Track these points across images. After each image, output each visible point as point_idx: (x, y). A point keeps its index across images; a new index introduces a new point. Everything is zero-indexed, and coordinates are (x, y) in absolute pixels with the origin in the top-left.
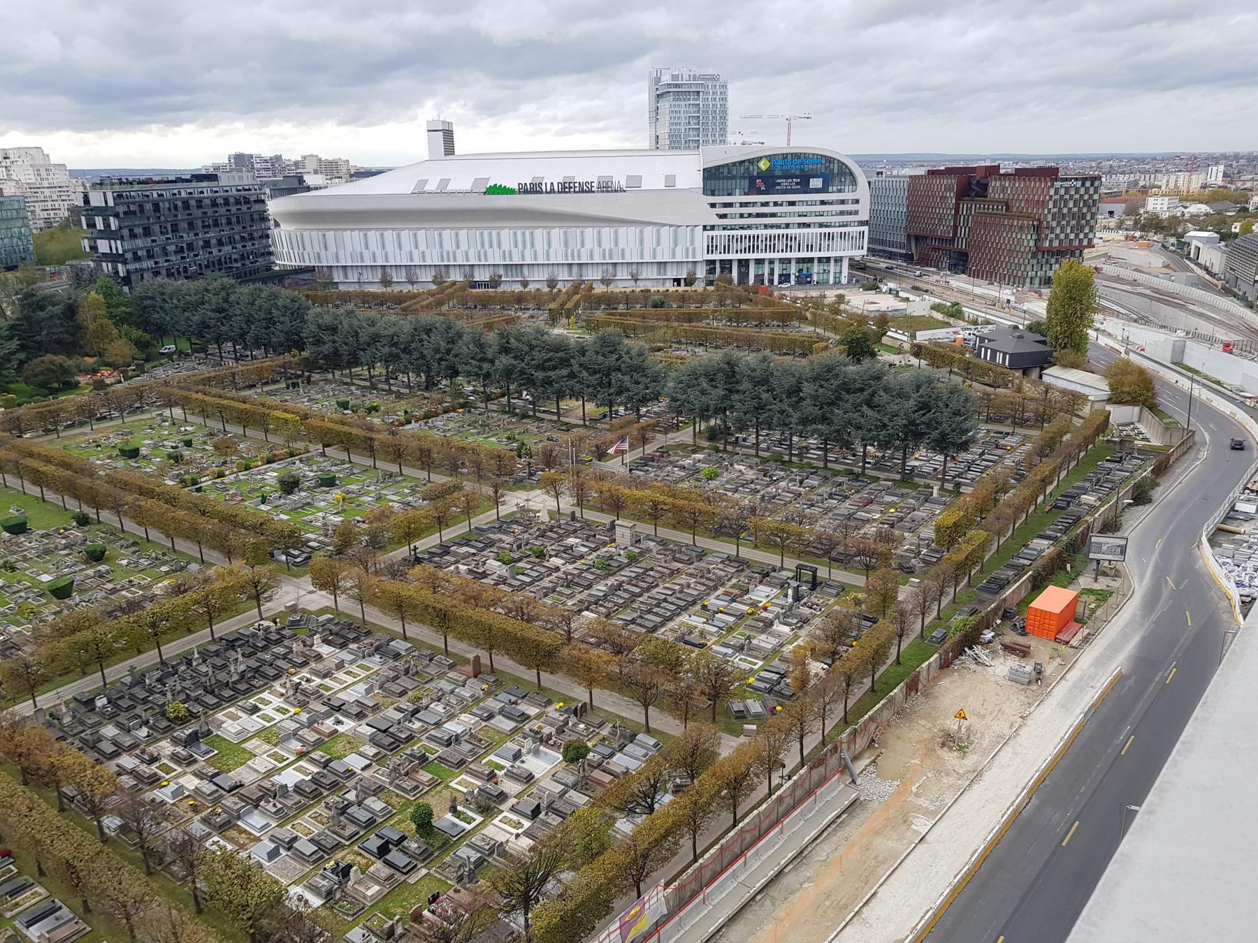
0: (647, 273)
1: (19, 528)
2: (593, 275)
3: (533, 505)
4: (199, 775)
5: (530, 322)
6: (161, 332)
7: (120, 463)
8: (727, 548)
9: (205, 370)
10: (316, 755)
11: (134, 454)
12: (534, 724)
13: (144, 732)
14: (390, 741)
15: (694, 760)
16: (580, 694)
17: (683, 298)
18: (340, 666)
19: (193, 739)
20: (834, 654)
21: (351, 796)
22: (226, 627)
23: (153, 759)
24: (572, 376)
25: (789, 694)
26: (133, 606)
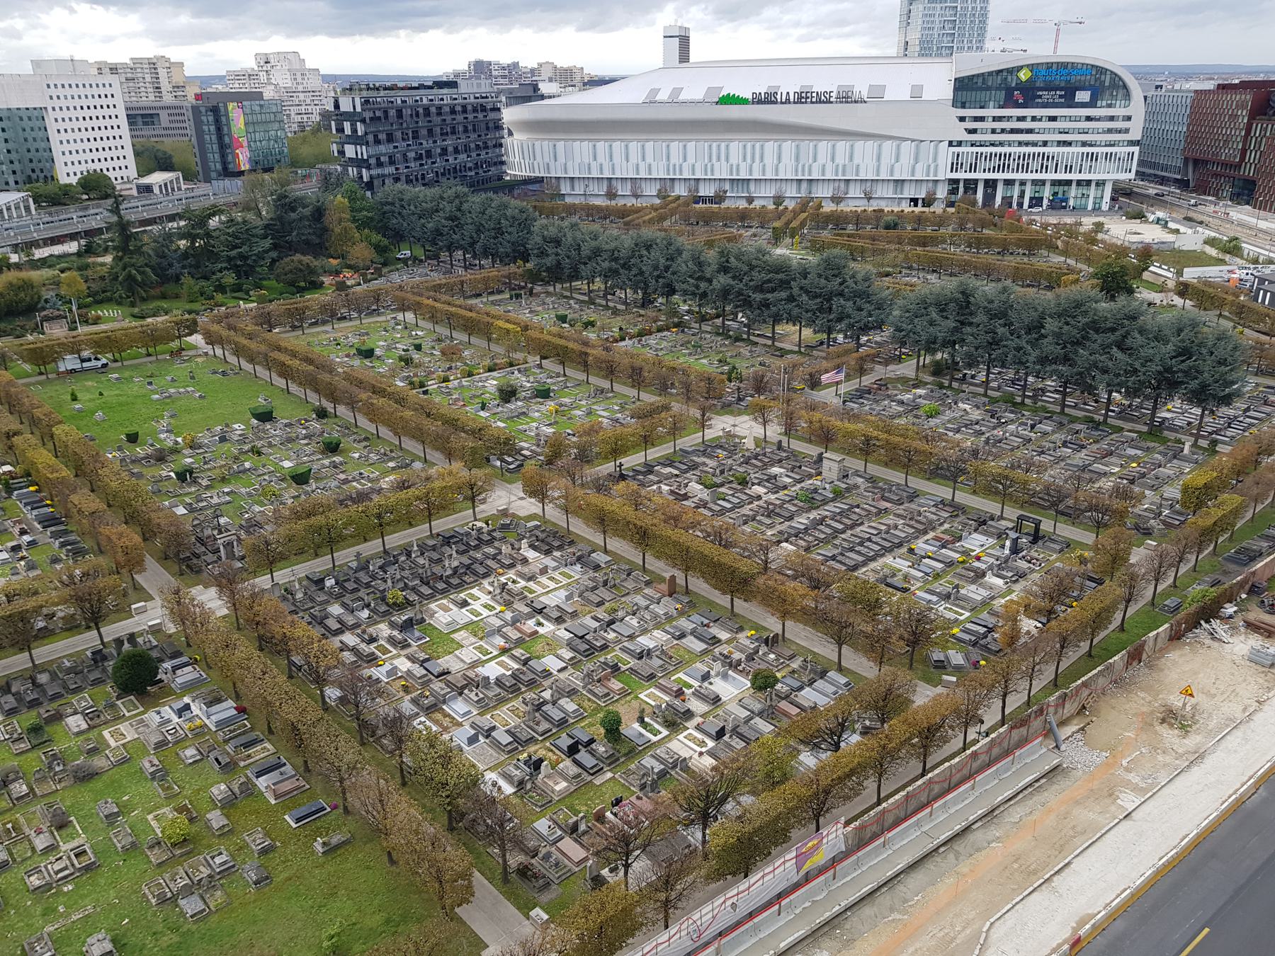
0: (881, 191)
1: (265, 416)
2: (823, 192)
3: (739, 431)
4: (412, 659)
5: (752, 240)
7: (357, 362)
8: (944, 491)
9: (437, 277)
10: (518, 652)
11: (369, 354)
12: (725, 649)
13: (365, 614)
14: (585, 648)
15: (887, 704)
16: (773, 624)
17: (919, 220)
18: (544, 571)
19: (408, 625)
20: (1050, 613)
21: (547, 695)
22: (443, 524)
23: (372, 640)
24: (791, 299)
25: (996, 651)
26: (362, 497)
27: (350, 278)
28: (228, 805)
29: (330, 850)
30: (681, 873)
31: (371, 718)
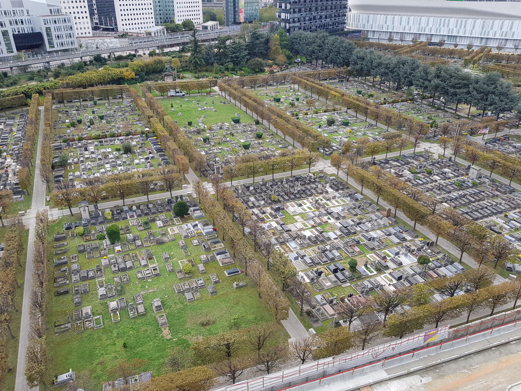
1: (237, 121)
4: (277, 223)
7: (273, 103)
10: (319, 228)
11: (278, 100)
13: (263, 202)
18: (334, 198)
19: (278, 210)
21: (328, 247)
22: (297, 172)
23: (264, 213)
26: (267, 157)
28: (206, 263)
29: (239, 287)
31: (259, 242)
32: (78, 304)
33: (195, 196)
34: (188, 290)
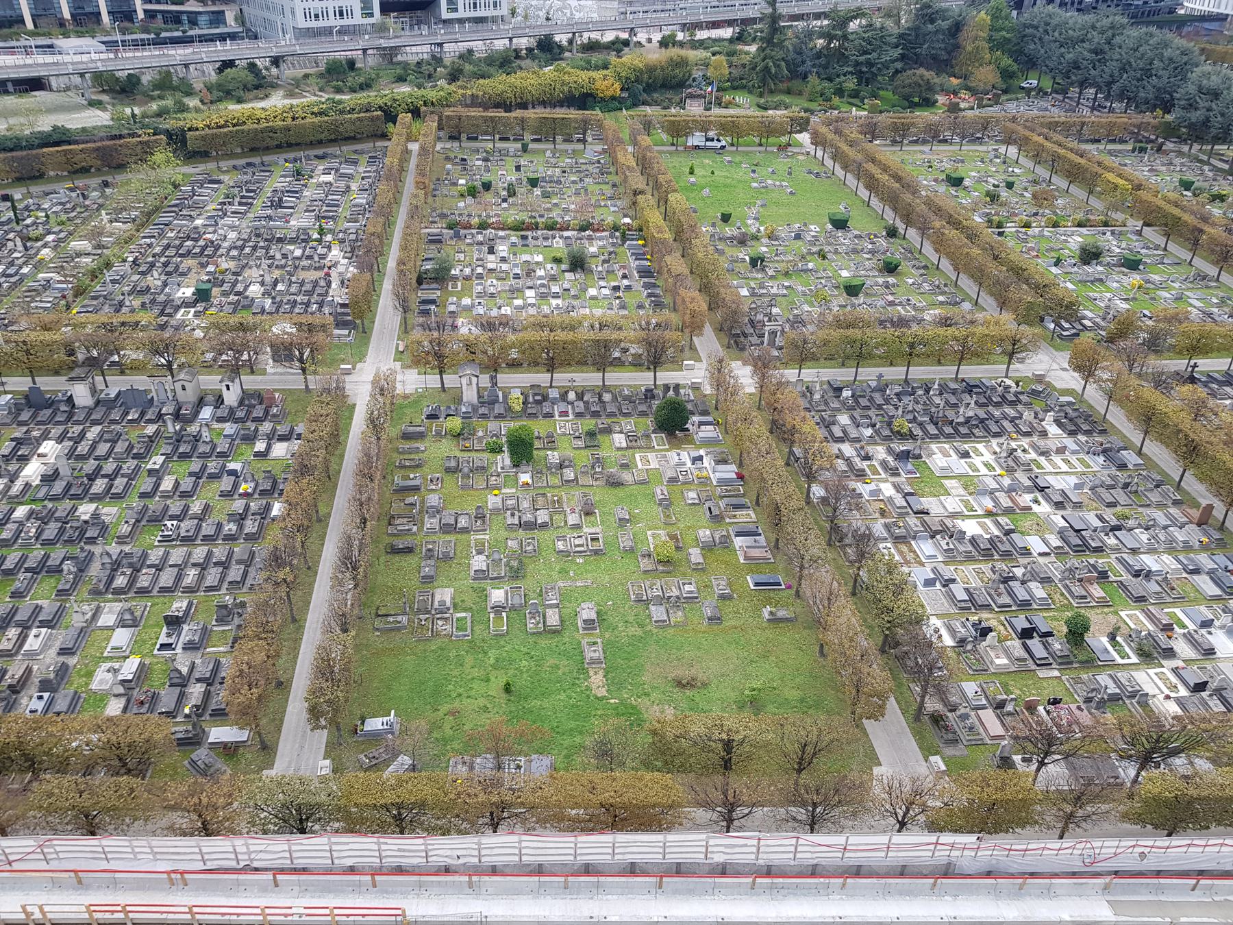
4: (897, 488)
6: (1030, 63)
7: (942, 188)
9: (1057, 114)
11: (957, 182)
13: (869, 432)
19: (904, 456)
23: (867, 458)
26: (902, 322)
27: (965, 101)
28: (708, 548)
30: (1097, 798)
31: (843, 525)
32: (429, 580)
33: (708, 390)
34: (660, 600)
